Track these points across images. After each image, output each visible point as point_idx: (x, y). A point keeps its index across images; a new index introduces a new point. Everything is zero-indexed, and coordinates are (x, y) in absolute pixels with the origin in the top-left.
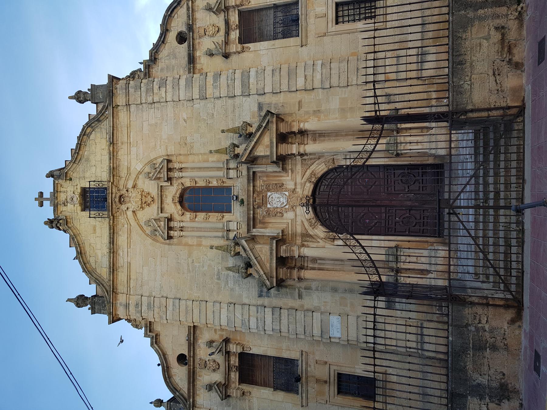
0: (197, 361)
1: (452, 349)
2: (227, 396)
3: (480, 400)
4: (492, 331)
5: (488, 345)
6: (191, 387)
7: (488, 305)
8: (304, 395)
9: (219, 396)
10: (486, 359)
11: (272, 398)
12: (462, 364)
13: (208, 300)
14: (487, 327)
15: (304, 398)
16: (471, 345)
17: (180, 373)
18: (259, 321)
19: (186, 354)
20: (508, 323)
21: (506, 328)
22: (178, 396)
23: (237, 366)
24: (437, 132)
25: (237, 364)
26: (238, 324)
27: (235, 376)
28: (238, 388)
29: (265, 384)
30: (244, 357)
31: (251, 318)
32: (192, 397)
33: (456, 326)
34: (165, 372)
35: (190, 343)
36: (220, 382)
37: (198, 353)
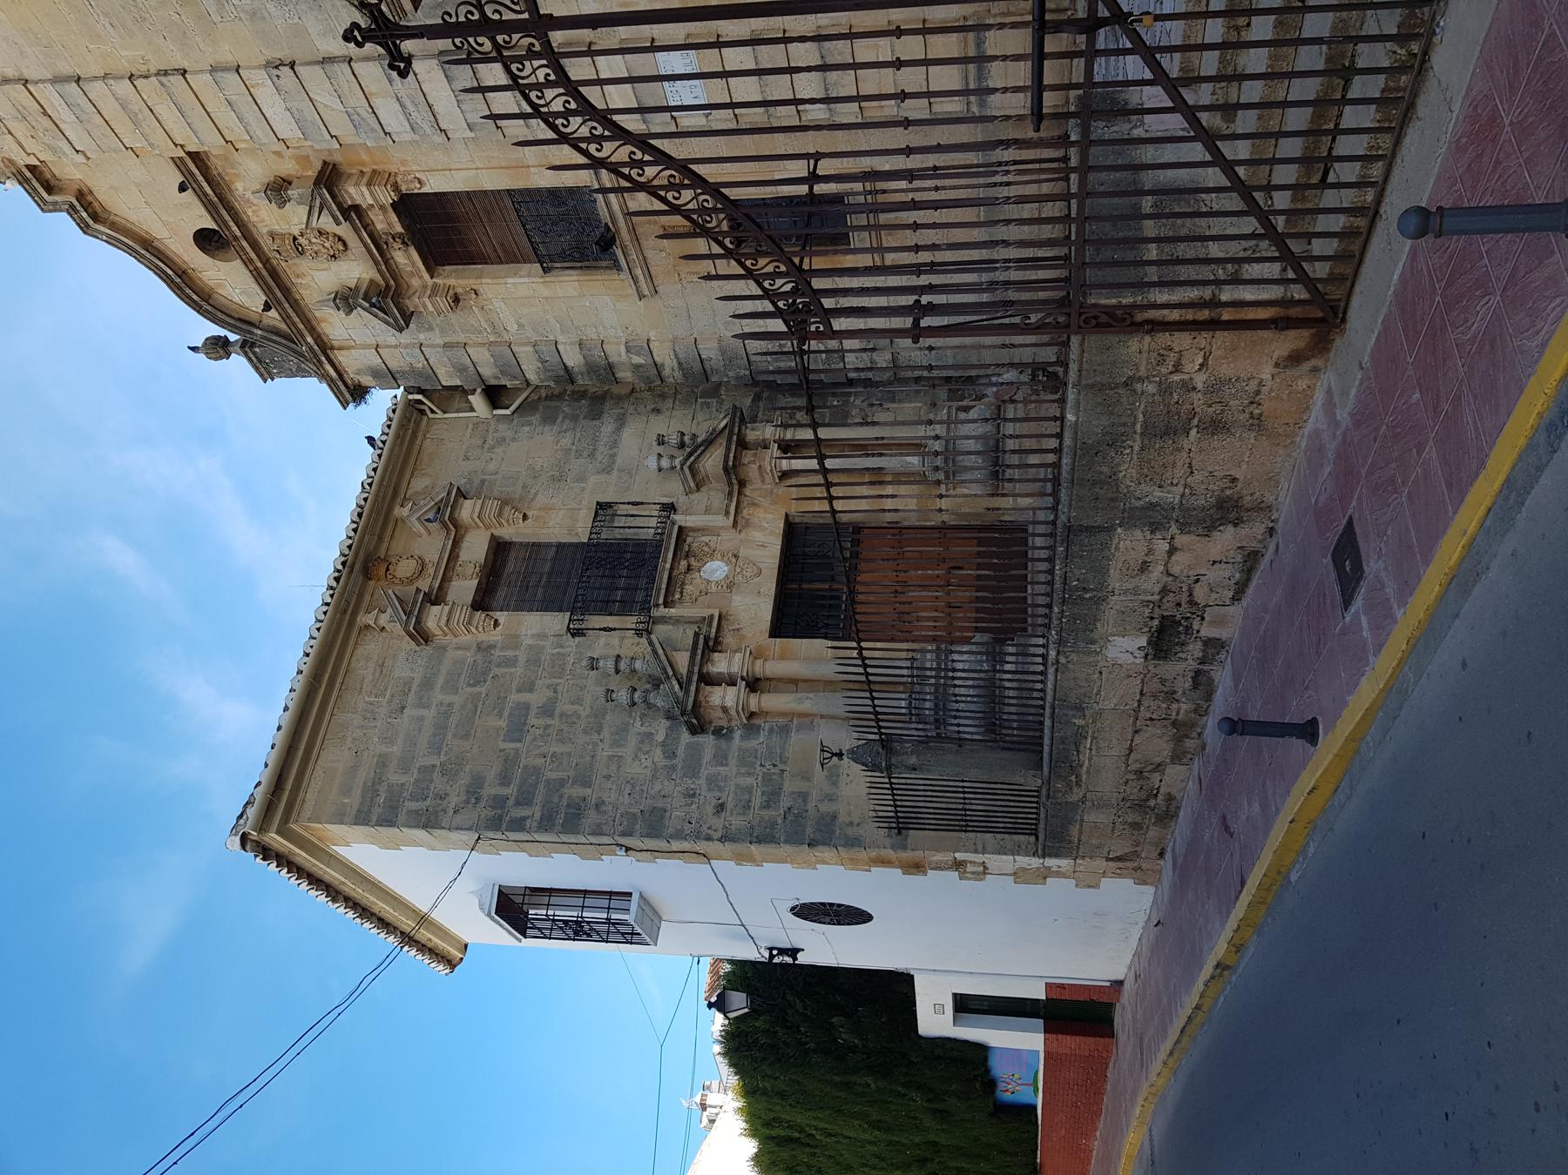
0: (267, 244)
1: (1075, 439)
2: (407, 317)
3: (1152, 532)
4: (1214, 388)
5: (1195, 421)
6: (290, 311)
7: (1214, 325)
8: (639, 272)
9: (387, 323)
10: (1184, 454)
11: (546, 293)
12: (1106, 470)
13: (185, 64)
14: (1200, 380)
15: (641, 277)
16: (1138, 427)
17: (232, 281)
18: (411, 108)
19: (213, 226)
20: (1277, 365)
21: (1266, 376)
22: (263, 337)
23: (400, 235)
24: (1018, 178)
25: (399, 229)
26: (341, 127)
27: (407, 259)
28: (435, 288)
29: (510, 257)
30: (410, 206)
31: (376, 102)
32: (305, 333)
33: (1092, 386)
34: (180, 289)
35: (211, 202)
36: (372, 281)
37: (254, 219)
